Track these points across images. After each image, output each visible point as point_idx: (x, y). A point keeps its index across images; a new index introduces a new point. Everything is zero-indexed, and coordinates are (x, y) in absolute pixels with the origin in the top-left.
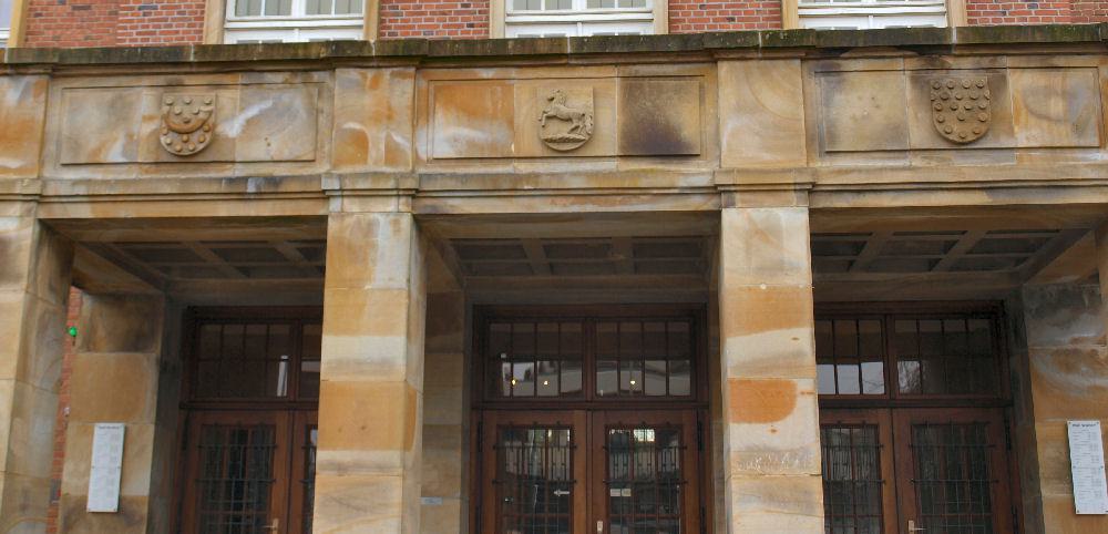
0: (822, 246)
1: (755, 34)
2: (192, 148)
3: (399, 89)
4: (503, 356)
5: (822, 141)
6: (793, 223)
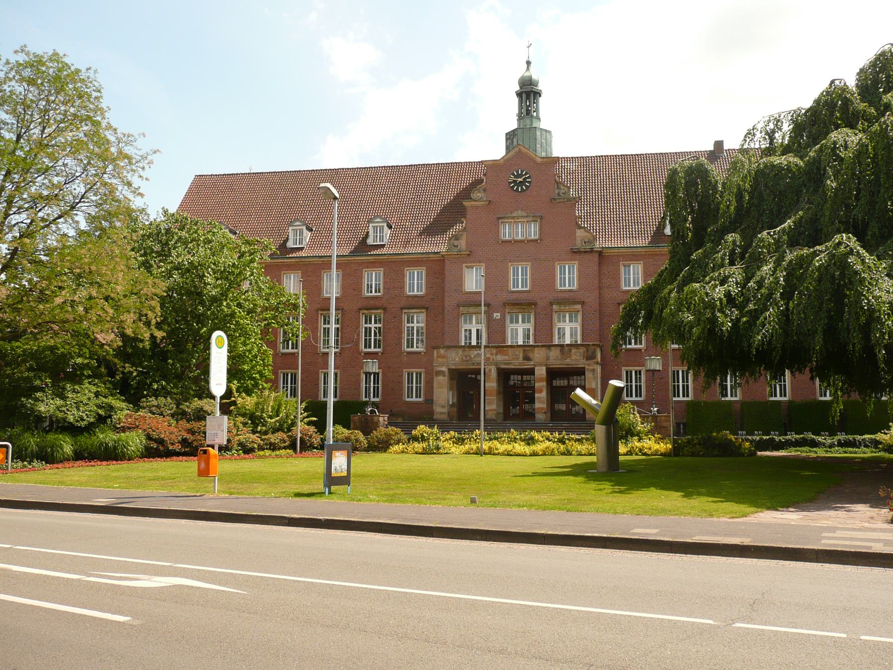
0: (547, 372)
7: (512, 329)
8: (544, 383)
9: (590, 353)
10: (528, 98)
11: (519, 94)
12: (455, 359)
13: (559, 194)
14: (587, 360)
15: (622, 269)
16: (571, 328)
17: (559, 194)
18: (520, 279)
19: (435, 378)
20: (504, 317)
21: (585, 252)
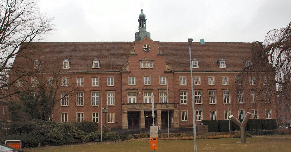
0: (162, 112)
1: (146, 118)
2: (134, 108)
3: (144, 105)
4: (147, 117)
5: (162, 108)
6: (160, 111)
7: (129, 98)
8: (161, 116)
9: (175, 106)
10: (143, 21)
11: (138, 20)
12: (127, 109)
13: (160, 53)
14: (174, 108)
15: (180, 78)
16: (165, 98)
17: (160, 53)
18: (147, 81)
19: (123, 115)
20: (143, 94)
21: (169, 73)
